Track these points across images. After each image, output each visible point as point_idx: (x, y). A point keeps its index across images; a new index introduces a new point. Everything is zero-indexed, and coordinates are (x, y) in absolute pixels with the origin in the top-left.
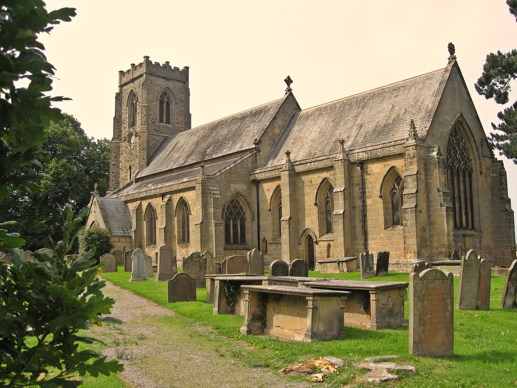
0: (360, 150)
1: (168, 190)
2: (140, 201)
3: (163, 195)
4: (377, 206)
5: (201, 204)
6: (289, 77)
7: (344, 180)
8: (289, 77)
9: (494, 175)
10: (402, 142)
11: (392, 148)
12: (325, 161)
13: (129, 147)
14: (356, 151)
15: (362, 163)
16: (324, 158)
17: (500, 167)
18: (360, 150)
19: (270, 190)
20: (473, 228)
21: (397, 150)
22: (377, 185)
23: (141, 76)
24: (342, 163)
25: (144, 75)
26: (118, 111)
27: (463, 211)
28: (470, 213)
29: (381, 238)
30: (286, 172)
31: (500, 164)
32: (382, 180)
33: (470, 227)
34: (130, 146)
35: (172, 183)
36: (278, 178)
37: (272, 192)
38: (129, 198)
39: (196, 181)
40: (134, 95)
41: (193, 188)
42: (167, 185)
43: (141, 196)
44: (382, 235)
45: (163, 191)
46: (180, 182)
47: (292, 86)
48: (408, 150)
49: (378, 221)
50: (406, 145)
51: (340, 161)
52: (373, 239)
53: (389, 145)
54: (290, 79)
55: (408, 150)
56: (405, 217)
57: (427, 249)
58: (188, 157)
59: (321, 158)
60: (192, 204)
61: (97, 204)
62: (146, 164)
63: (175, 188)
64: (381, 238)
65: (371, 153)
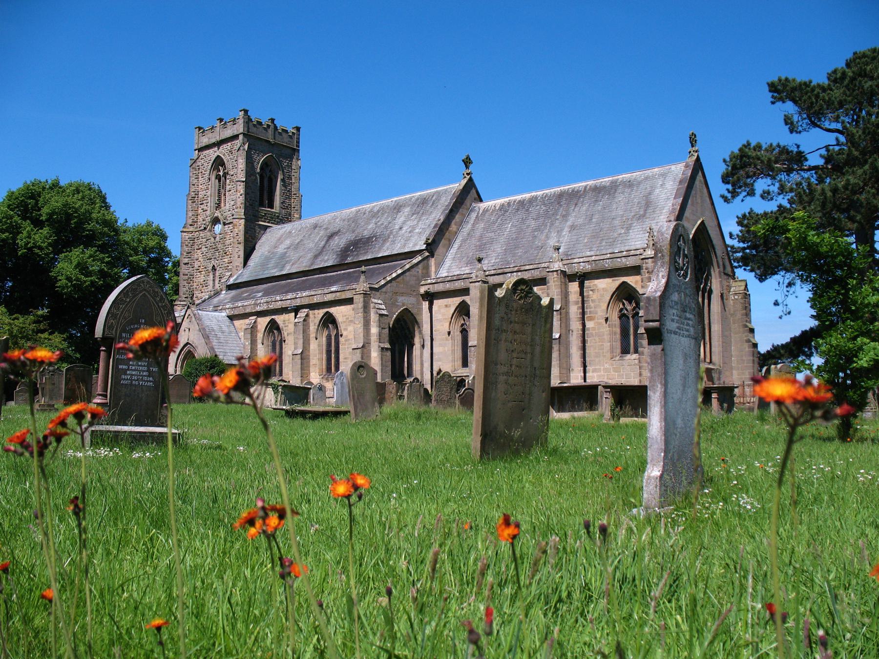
0: (581, 260)
1: (306, 301)
2: (255, 317)
3: (296, 310)
4: (602, 330)
5: (362, 322)
6: (468, 158)
7: (560, 297)
8: (468, 158)
9: (736, 297)
10: (638, 252)
11: (624, 260)
12: (533, 271)
13: (213, 239)
14: (575, 261)
15: (582, 278)
16: (531, 267)
17: (743, 288)
18: (581, 260)
19: (450, 306)
20: (711, 362)
21: (630, 262)
22: (602, 304)
23: (235, 137)
24: (557, 274)
25: (241, 137)
26: (194, 185)
27: (333, 356)
28: (708, 343)
29: (606, 370)
30: (477, 283)
31: (743, 284)
32: (609, 298)
33: (708, 360)
34: (215, 238)
35: (313, 293)
36: (465, 291)
37: (454, 308)
38: (236, 313)
39: (354, 291)
40: (223, 164)
41: (349, 301)
42: (304, 294)
43: (258, 309)
44: (607, 366)
45: (298, 302)
46: (326, 291)
47: (472, 168)
48: (646, 263)
49: (603, 349)
50: (643, 257)
51: (555, 273)
52: (594, 371)
53: (619, 254)
54: (470, 159)
55: (646, 263)
56: (641, 343)
57: (85, 450)
58: (316, 257)
59: (527, 267)
60: (344, 322)
61: (194, 319)
62: (242, 265)
63: (316, 300)
64: (606, 370)
65: (596, 265)
